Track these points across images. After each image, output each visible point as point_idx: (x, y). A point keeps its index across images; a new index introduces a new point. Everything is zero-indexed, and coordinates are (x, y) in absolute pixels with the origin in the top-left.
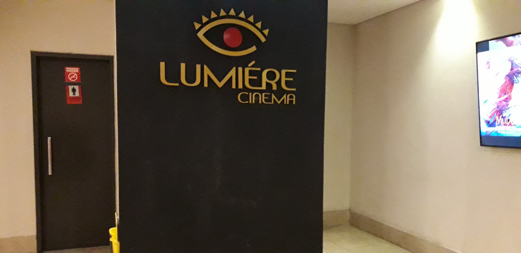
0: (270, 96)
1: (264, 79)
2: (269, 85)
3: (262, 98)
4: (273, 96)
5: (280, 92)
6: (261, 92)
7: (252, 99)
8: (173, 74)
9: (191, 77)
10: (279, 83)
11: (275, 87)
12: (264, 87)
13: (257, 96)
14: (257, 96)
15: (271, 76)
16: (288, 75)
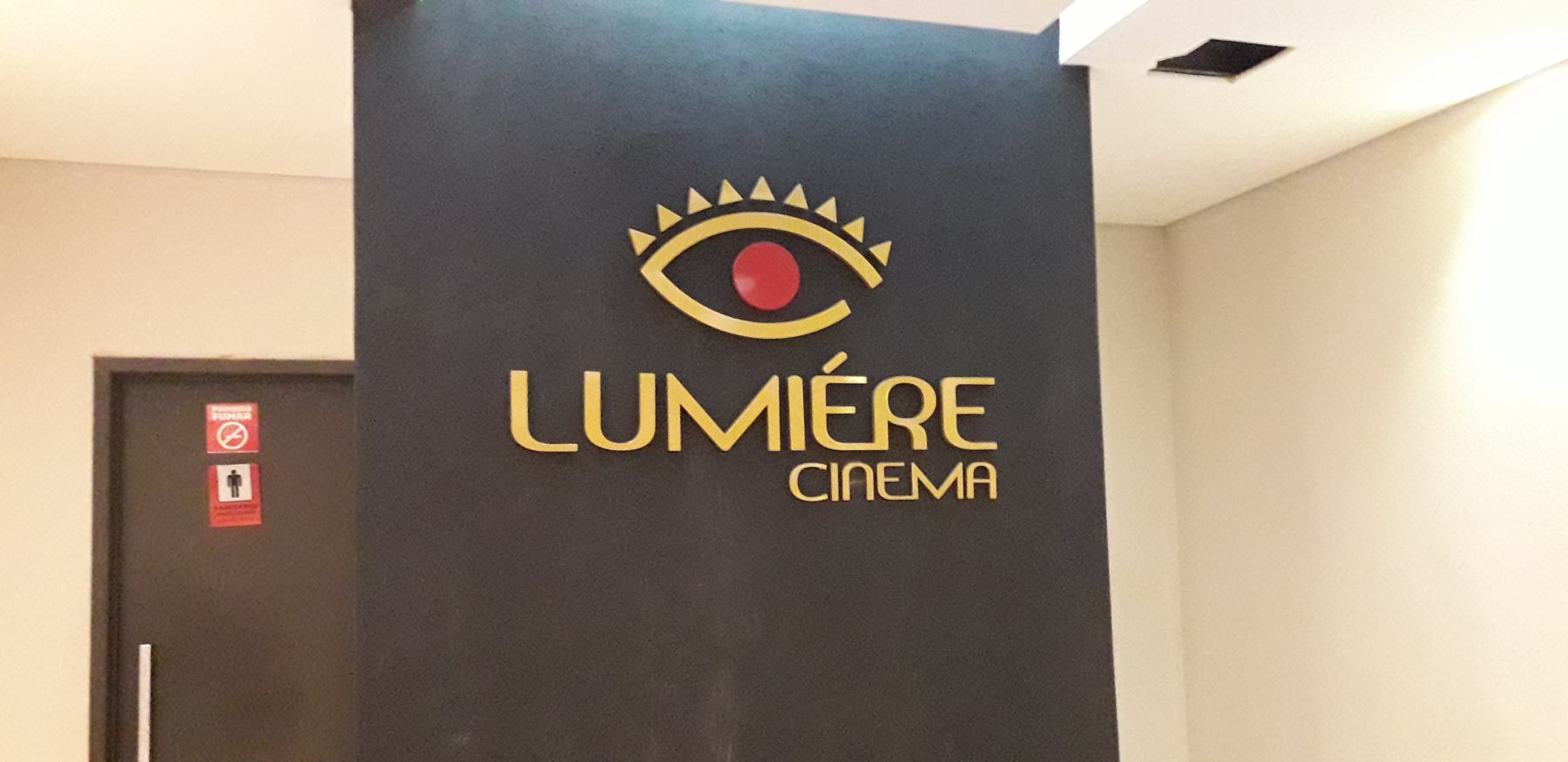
0: (906, 474)
1: (883, 414)
2: (899, 436)
3: (877, 482)
4: (917, 473)
5: (940, 457)
6: (873, 458)
7: (841, 485)
8: (554, 413)
9: (620, 419)
10: (934, 426)
11: (920, 441)
12: (881, 442)
13: (858, 474)
14: (858, 474)
15: (906, 401)
16: (964, 396)
